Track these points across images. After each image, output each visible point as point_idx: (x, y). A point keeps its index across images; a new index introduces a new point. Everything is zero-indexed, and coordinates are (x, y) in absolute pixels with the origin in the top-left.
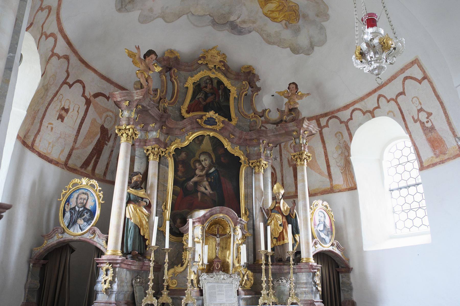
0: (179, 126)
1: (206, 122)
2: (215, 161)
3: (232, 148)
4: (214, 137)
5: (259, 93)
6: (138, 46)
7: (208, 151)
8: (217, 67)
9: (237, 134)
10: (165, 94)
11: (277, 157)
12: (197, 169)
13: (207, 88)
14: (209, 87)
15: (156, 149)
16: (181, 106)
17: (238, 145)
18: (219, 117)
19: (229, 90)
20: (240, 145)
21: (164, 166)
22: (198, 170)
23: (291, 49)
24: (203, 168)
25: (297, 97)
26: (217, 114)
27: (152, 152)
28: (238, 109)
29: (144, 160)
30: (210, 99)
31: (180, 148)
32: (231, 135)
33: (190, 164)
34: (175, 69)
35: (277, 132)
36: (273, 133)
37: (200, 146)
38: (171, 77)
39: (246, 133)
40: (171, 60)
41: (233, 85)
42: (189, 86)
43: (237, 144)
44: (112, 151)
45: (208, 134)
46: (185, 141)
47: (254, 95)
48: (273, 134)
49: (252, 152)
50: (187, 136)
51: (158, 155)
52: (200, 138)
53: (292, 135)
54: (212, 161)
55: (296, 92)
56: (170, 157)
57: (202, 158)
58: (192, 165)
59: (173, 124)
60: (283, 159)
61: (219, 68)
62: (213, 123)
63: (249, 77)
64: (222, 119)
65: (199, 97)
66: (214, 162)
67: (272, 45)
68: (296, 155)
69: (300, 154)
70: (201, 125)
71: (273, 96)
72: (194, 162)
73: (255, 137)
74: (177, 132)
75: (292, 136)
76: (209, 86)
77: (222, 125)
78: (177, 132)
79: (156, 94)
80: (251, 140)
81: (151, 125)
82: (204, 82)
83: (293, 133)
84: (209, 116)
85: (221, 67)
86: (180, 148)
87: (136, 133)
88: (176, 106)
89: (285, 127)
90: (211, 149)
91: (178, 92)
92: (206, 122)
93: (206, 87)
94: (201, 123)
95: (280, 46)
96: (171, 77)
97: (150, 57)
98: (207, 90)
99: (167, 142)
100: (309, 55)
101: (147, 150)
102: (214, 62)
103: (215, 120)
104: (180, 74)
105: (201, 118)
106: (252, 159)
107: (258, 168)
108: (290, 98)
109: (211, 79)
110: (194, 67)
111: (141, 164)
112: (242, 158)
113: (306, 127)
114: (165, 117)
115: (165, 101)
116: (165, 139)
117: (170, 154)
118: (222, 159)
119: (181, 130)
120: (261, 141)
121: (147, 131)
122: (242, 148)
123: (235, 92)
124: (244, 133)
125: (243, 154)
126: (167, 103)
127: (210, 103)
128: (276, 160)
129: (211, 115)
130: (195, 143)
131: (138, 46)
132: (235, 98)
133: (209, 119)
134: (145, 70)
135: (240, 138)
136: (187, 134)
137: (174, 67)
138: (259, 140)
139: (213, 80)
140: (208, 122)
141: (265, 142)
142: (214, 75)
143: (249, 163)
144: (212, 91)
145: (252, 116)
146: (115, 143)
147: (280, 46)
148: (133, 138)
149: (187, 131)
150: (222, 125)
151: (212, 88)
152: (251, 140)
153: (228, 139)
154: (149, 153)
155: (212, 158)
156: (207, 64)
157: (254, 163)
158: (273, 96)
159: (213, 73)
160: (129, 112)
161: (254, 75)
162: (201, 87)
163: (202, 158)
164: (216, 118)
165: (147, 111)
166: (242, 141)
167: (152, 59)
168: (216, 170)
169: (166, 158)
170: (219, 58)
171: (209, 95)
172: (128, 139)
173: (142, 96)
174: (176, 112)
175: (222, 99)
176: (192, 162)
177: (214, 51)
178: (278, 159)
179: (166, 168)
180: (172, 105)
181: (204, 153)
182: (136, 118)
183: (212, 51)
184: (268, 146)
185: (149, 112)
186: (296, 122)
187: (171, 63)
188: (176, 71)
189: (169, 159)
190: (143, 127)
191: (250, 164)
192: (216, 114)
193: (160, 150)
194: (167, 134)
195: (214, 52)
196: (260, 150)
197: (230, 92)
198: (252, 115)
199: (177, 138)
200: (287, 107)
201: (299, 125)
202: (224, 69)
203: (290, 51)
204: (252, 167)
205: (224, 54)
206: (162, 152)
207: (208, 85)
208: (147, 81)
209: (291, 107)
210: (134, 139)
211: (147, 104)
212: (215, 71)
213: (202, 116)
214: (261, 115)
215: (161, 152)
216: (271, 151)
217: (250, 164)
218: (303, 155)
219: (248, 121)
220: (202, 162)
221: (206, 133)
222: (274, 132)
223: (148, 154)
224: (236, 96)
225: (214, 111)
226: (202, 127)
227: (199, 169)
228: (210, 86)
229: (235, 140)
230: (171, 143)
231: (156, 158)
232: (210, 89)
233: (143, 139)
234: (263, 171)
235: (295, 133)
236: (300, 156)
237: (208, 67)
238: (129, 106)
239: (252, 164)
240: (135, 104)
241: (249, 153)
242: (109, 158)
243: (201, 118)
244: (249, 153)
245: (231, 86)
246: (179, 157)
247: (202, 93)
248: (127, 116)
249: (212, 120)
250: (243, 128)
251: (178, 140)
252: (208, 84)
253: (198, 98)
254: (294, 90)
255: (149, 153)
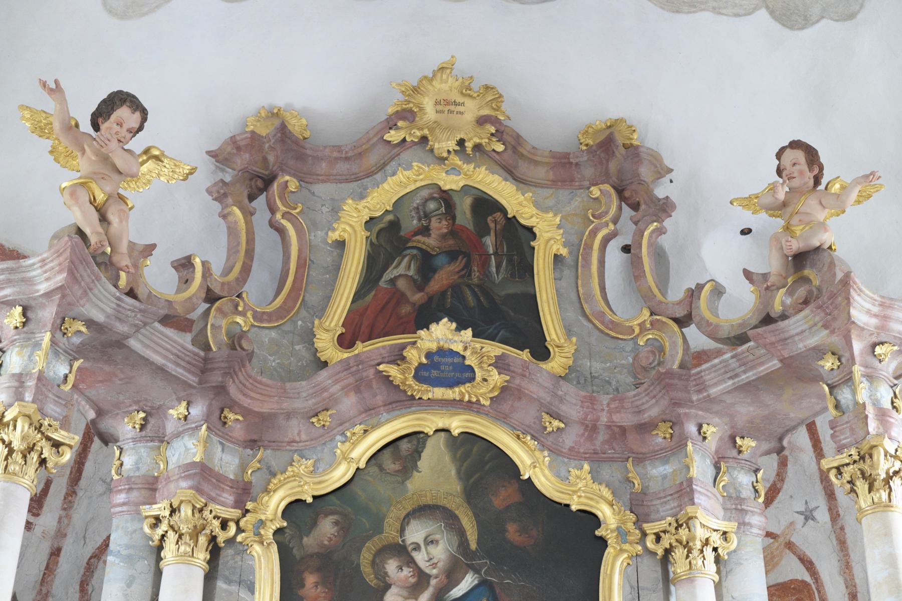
0: (298, 404)
1: (422, 374)
2: (479, 542)
3: (558, 475)
4: (469, 437)
5: (668, 223)
6: (56, 82)
7: (444, 502)
8: (469, 145)
9: (573, 411)
10: (237, 279)
11: (812, 505)
12: (388, 587)
13: (429, 235)
14: (440, 229)
15: (186, 511)
16: (316, 322)
17: (586, 459)
18: (478, 344)
19: (530, 230)
20: (596, 458)
21: (234, 588)
22: (394, 590)
23: (772, 13)
24: (422, 579)
25: (821, 203)
26: (469, 332)
27: (172, 527)
28: (578, 305)
29: (145, 565)
30: (441, 280)
31: (310, 500)
32: (546, 418)
33: (358, 566)
34: (287, 178)
35: (745, 372)
36: (731, 378)
37: (403, 482)
38: (273, 210)
39: (613, 400)
40: (267, 146)
41: (543, 208)
42: (346, 236)
43: (575, 455)
44: (56, 553)
45: (441, 425)
46: (333, 465)
47: (646, 233)
48: (730, 382)
49: (654, 487)
50: (343, 442)
51: (203, 540)
52: (404, 446)
53: (816, 378)
54: (463, 543)
55: (817, 181)
56: (262, 543)
57: (416, 533)
58: (366, 569)
59: (270, 396)
60: (841, 512)
61: (478, 147)
62: (458, 375)
63: (613, 166)
64: (494, 349)
65: (396, 273)
66: (473, 546)
67: (689, 12)
68: (847, 465)
69: (862, 458)
70: (405, 392)
71: (746, 232)
72: (375, 556)
73: (653, 412)
74: (296, 432)
75: (822, 379)
76: (438, 226)
77: (496, 378)
78: (295, 429)
79: (187, 281)
80: (646, 428)
81: (171, 411)
82: (413, 213)
83: (821, 363)
84: (434, 346)
85: (484, 141)
86: (310, 500)
87: (55, 436)
88: (295, 322)
89: (773, 339)
90: (457, 487)
91: (301, 265)
92: (426, 374)
93: (425, 231)
94: (403, 383)
95: (724, 11)
96: (273, 210)
97: (114, 117)
98: (431, 242)
99: (254, 479)
100: (851, 16)
101: (153, 521)
102: (450, 129)
103: (464, 357)
104: (313, 194)
105: (398, 357)
106: (658, 516)
107: (687, 557)
108: (789, 210)
109: (446, 198)
110: (373, 159)
111: (129, 586)
112: (604, 511)
113: (874, 321)
114: (218, 368)
115: (237, 306)
116: (243, 468)
117: (262, 532)
118: (512, 531)
119: (314, 420)
120: (692, 429)
121: (162, 442)
122: (607, 471)
123: (558, 235)
124: (605, 402)
125: (610, 497)
126: (249, 314)
127: (443, 293)
128: (813, 519)
129: (438, 341)
130: (381, 468)
131: (56, 82)
132: (557, 258)
133: (436, 359)
134: (95, 173)
135: (591, 429)
136: (343, 434)
137: (283, 171)
138: (675, 423)
139: (456, 199)
140: (435, 373)
141: (709, 430)
142: (456, 178)
143: (644, 535)
144: (451, 242)
145: (642, 325)
146: (69, 517)
147: (724, 11)
148: (43, 462)
149: (341, 424)
150: (496, 378)
151: (454, 232)
152: (646, 428)
153: (534, 438)
154: (160, 531)
155: (461, 533)
156: (424, 139)
157: (665, 532)
158: (746, 232)
159: (455, 170)
160: (27, 352)
161: (633, 151)
162: (402, 233)
163: (416, 533)
164: (465, 349)
165: (120, 344)
166: (602, 436)
167: (120, 124)
168: (483, 583)
169: (243, 550)
170: (471, 110)
171: (441, 260)
172: (11, 468)
173: (65, 275)
174: (297, 347)
175: (497, 272)
176: (366, 557)
177: (446, 82)
178: (823, 515)
179: (242, 595)
180: (277, 320)
181: (423, 511)
182: (66, 377)
183: (436, 83)
184: (734, 453)
185: (129, 348)
186: (820, 307)
187: (271, 158)
188: (293, 185)
189: (257, 549)
190: (142, 427)
191: (650, 543)
192: (463, 332)
193: (206, 513)
194: (253, 444)
195: (445, 87)
196: (688, 468)
197: (534, 236)
198: (640, 321)
199: (296, 457)
200: (774, 251)
201: (834, 319)
202: (500, 148)
203: (773, 21)
204: (660, 552)
205: (487, 88)
206: (224, 525)
207: (434, 223)
208: (103, 219)
209: (796, 246)
210: (50, 465)
211: (109, 310)
212: (460, 163)
213: (403, 347)
214: (680, 313)
215: (216, 523)
216: (756, 471)
217: (650, 543)
218: (875, 457)
219: (628, 349)
220: (415, 554)
221: (433, 422)
222: (736, 376)
223: (157, 537)
224: (564, 252)
225: (451, 320)
226: (412, 397)
227: (402, 587)
228: (444, 222)
229: (570, 439)
230: (269, 482)
231: (189, 549)
232: (444, 237)
233: (144, 476)
234: (711, 567)
235: (828, 363)
236: (866, 467)
237: (432, 150)
238: (25, 329)
239: (658, 539)
240: (48, 314)
241: (644, 493)
242: (43, 581)
243: (398, 357)
244: (644, 493)
245: (534, 211)
246: (305, 539)
247: (406, 260)
248: (17, 371)
249: (450, 360)
250: (609, 383)
251: (302, 467)
252: (434, 220)
253: (393, 281)
254: (801, 173)
255: (160, 531)
